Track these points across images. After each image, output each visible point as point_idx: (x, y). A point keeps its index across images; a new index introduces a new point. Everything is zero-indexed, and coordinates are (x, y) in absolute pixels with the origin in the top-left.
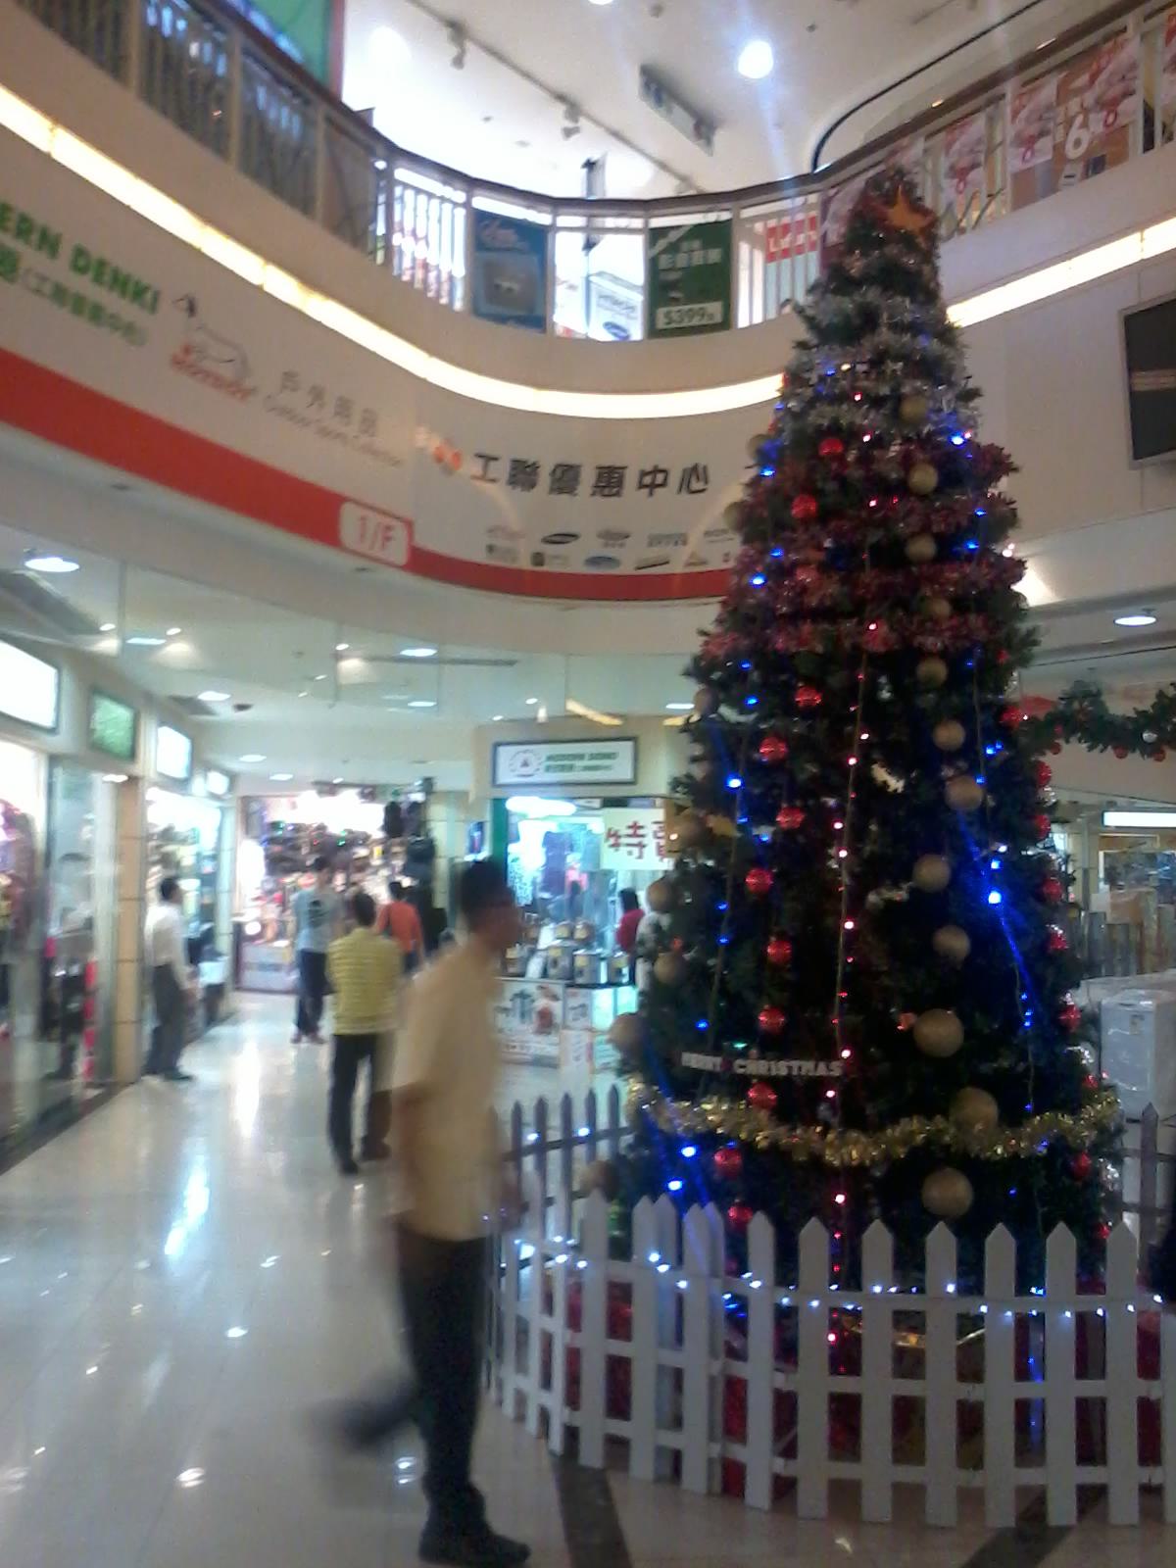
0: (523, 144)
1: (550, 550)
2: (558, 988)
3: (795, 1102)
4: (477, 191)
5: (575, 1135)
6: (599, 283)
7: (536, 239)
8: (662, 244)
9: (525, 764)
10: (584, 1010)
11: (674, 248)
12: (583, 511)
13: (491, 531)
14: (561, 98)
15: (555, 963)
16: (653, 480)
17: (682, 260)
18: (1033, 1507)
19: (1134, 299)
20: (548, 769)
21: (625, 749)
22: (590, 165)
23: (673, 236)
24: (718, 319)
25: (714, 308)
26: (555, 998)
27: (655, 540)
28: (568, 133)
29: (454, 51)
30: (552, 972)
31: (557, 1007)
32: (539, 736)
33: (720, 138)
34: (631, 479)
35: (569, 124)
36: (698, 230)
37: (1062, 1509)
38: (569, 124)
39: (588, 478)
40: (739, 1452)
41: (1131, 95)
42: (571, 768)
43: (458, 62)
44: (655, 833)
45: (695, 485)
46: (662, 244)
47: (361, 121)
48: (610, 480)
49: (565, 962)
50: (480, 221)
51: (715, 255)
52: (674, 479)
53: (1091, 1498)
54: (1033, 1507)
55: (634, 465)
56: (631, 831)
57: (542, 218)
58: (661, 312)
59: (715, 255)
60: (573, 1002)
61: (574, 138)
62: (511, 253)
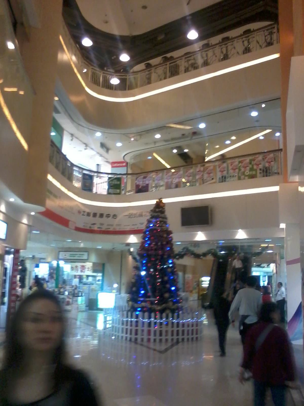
0: (75, 148)
1: (92, 226)
2: (71, 297)
3: (152, 303)
4: (83, 170)
6: (101, 186)
7: (91, 177)
8: (110, 180)
9: (65, 255)
10: (77, 301)
11: (112, 181)
12: (98, 220)
13: (84, 223)
14: (85, 144)
15: (71, 292)
16: (108, 216)
17: (113, 183)
18: (178, 339)
19: (184, 206)
20: (70, 256)
21: (86, 254)
22: (98, 165)
23: (112, 179)
24: (119, 192)
25: (118, 191)
26: (70, 299)
27: (108, 225)
28: (86, 149)
29: (71, 138)
30: (70, 294)
31: (71, 300)
32: (63, 250)
33: (110, 152)
34: (105, 215)
35: (85, 148)
36: (116, 178)
37: (180, 340)
38: (85, 148)
39: (98, 215)
40: (150, 337)
41: (177, 147)
42: (74, 257)
43: (72, 140)
44: (80, 268)
45: (115, 218)
46: (110, 180)
47: (65, 156)
48: (101, 215)
49: (73, 292)
50: (84, 174)
51: (118, 183)
52: (112, 216)
53: (183, 339)
54: (178, 339)
55: (105, 213)
56: (75, 267)
57: (92, 174)
58: (110, 190)
59: (118, 183)
60: (74, 299)
61: (86, 150)
62: (88, 181)
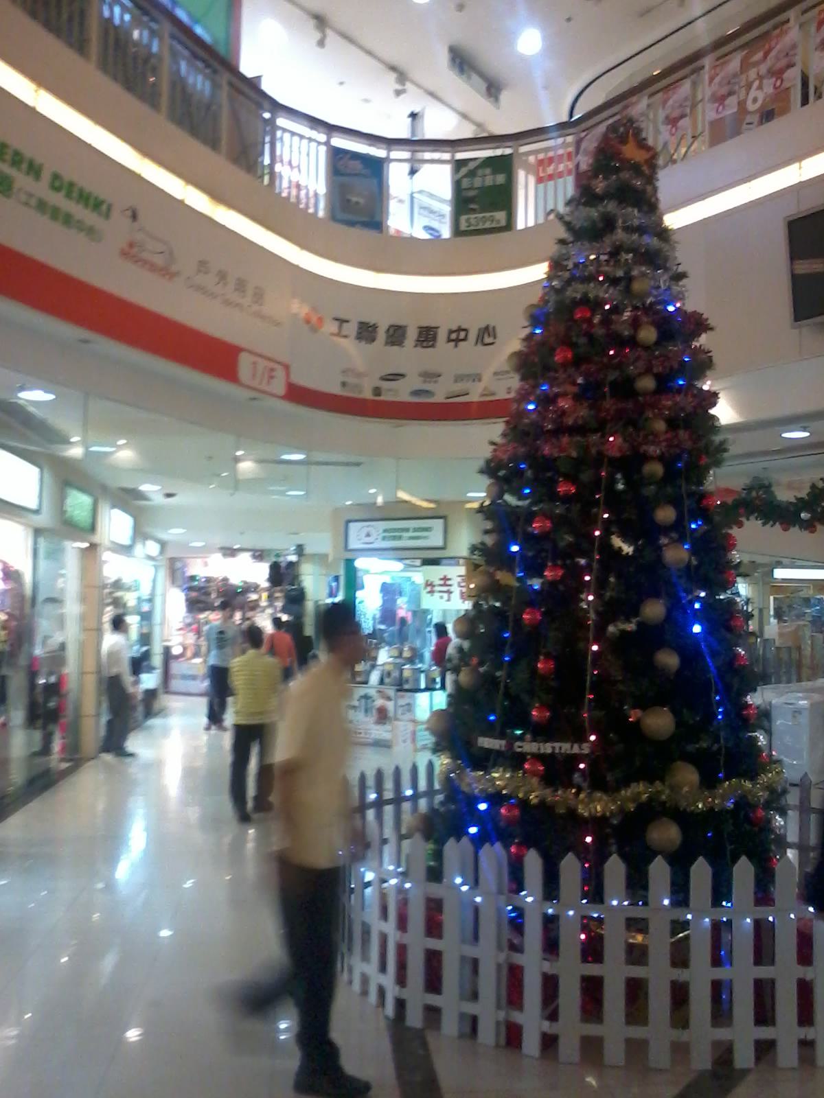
0: (366, 101)
1: (385, 385)
2: (391, 692)
3: (557, 772)
4: (334, 134)
6: (419, 198)
7: (376, 168)
8: (464, 171)
9: (368, 535)
10: (410, 707)
11: (472, 174)
12: (408, 358)
13: (344, 372)
14: (393, 68)
15: (389, 674)
16: (458, 336)
17: (478, 182)
18: (724, 1056)
19: (795, 209)
20: (384, 538)
21: (438, 524)
22: (413, 116)
23: (472, 165)
24: (503, 223)
25: (501, 216)
26: (389, 699)
27: (459, 378)
28: (398, 93)
29: (318, 36)
30: (387, 680)
31: (390, 705)
32: (377, 516)
33: (504, 96)
34: (442, 335)
35: (399, 87)
36: (489, 161)
37: (744, 1057)
38: (399, 87)
39: (412, 334)
40: (517, 1017)
41: (792, 66)
42: (400, 538)
43: (321, 43)
44: (459, 583)
45: (487, 340)
46: (464, 171)
47: (253, 84)
48: (427, 336)
49: (396, 674)
50: (337, 155)
51: (501, 179)
52: (473, 336)
53: (765, 1049)
54: (724, 1056)
55: (444, 325)
56: (442, 582)
57: (380, 152)
58: (463, 218)
59: (501, 179)
60: (402, 702)
61: (402, 96)
62: (358, 177)
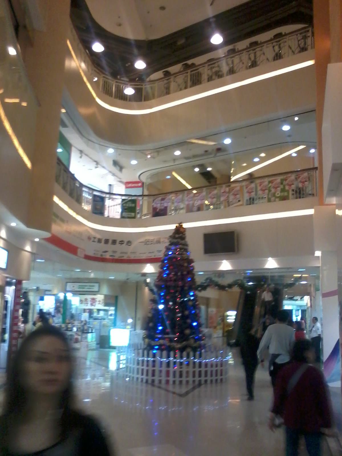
0: (84, 166)
1: (104, 254)
2: (80, 333)
3: (171, 340)
4: (94, 191)
5: (282, 309)
6: (113, 209)
7: (102, 199)
8: (124, 202)
9: (74, 287)
10: (86, 338)
11: (126, 203)
12: (110, 247)
13: (95, 250)
14: (95, 161)
15: (80, 328)
16: (122, 242)
17: (127, 205)
18: (200, 381)
19: (207, 231)
20: (79, 288)
21: (97, 285)
22: (110, 185)
23: (126, 201)
24: (133, 216)
25: (133, 214)
26: (79, 335)
27: (122, 253)
28: (96, 167)
29: (80, 155)
30: (79, 330)
31: (79, 337)
32: (71, 281)
33: (124, 170)
34: (118, 242)
35: (96, 166)
36: (130, 200)
37: (203, 382)
38: (96, 166)
39: (110, 242)
40: (169, 379)
41: (199, 165)
42: (84, 288)
43: (81, 157)
44: (90, 301)
45: (129, 244)
46: (124, 202)
47: (73, 175)
48: (114, 242)
49: (82, 328)
50: (95, 196)
51: (133, 205)
52: (125, 243)
53: (206, 381)
54: (200, 381)
55: (119, 239)
56: (84, 300)
57: (104, 195)
58: (124, 213)
59: (133, 205)
60: (84, 336)
61: (97, 169)
62: (99, 203)
